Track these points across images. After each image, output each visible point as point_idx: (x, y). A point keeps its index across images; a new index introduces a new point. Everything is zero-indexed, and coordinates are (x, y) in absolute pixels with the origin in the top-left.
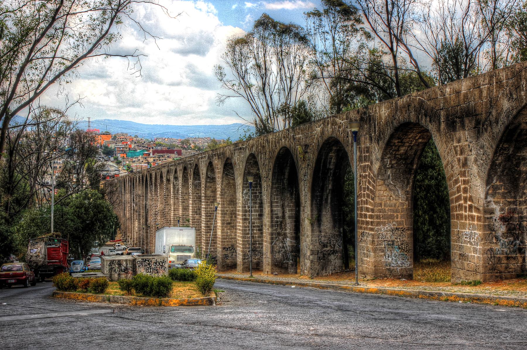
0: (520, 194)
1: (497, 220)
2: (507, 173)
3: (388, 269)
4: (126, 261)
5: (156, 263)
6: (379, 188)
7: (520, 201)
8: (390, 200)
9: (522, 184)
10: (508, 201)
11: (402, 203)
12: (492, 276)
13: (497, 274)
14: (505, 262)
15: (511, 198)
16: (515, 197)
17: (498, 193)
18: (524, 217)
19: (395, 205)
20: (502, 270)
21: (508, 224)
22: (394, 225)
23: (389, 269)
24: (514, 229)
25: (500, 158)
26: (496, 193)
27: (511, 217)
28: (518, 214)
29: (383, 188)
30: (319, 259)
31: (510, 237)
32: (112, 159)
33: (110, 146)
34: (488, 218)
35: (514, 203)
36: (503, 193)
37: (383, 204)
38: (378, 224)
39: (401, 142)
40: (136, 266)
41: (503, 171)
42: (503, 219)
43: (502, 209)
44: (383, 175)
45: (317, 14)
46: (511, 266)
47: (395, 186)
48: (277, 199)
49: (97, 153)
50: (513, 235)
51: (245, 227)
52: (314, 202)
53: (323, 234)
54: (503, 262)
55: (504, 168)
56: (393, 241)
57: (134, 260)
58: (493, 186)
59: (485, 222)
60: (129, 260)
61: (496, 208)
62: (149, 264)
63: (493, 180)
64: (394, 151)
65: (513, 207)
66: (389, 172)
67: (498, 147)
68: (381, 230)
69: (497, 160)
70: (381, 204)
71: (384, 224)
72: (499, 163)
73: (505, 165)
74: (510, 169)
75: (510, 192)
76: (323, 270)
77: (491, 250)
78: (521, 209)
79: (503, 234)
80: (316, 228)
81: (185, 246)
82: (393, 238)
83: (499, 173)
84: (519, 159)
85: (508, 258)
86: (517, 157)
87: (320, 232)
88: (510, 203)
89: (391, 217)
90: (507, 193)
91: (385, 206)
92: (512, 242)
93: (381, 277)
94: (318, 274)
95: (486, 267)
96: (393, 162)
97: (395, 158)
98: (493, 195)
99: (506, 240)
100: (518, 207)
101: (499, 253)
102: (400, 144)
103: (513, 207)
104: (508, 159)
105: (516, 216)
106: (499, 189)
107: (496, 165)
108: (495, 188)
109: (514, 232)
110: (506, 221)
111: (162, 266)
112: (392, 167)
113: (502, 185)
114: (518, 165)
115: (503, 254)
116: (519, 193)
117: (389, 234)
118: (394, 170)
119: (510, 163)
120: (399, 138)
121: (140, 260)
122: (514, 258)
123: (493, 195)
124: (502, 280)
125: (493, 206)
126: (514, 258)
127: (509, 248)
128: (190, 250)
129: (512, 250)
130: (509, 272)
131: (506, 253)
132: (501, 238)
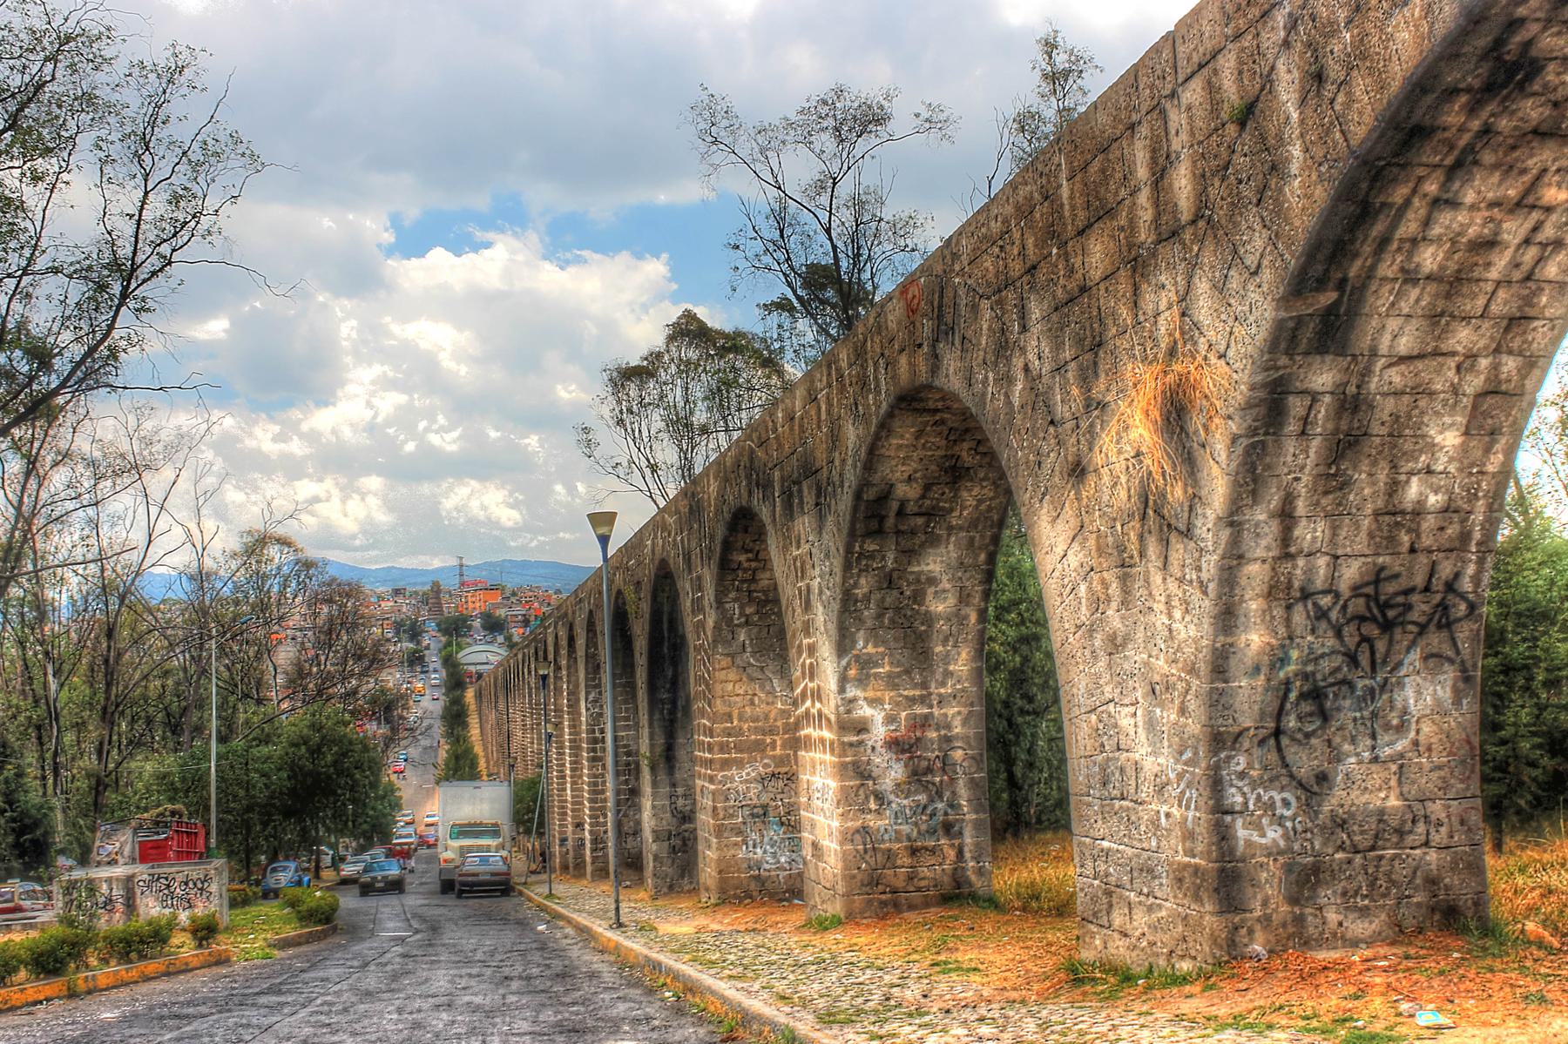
0: (939, 677)
1: (879, 749)
2: (892, 621)
3: (754, 877)
4: (109, 880)
5: (186, 884)
6: (721, 675)
7: (940, 695)
8: (752, 703)
9: (939, 649)
10: (907, 697)
11: (783, 711)
12: (870, 902)
13: (883, 897)
14: (907, 861)
15: (915, 686)
16: (924, 685)
17: (876, 675)
18: (957, 737)
19: (766, 717)
20: (900, 883)
21: (911, 758)
22: (766, 766)
23: (757, 878)
24: (929, 770)
25: (863, 581)
26: (868, 676)
27: (918, 740)
28: (937, 730)
29: (732, 675)
30: (673, 849)
31: (916, 792)
32: (500, 639)
33: (498, 613)
34: (851, 745)
35: (923, 700)
36: (890, 675)
37: (735, 715)
38: (726, 764)
39: (756, 559)
40: (134, 893)
41: (880, 616)
42: (894, 744)
43: (890, 719)
44: (727, 643)
45: (782, 306)
46: (924, 871)
47: (762, 668)
48: (627, 710)
49: (470, 628)
50: (925, 787)
51: (595, 776)
52: (657, 716)
53: (680, 790)
54: (899, 862)
55: (882, 610)
56: (765, 807)
57: (130, 878)
58: (857, 656)
59: (843, 754)
60: (117, 879)
61: (874, 716)
62: (168, 886)
63: (854, 642)
64: (743, 581)
65: (921, 710)
66: (742, 636)
67: (849, 550)
68: (732, 780)
69: (856, 585)
70: (729, 717)
71: (740, 764)
72: (864, 595)
73: (883, 599)
74: (898, 610)
75: (908, 672)
76: (682, 877)
77: (865, 830)
78: (946, 715)
79: (898, 785)
80: (662, 776)
81: (481, 824)
82: (765, 799)
83: (869, 623)
84: (918, 581)
85: (914, 852)
86: (911, 578)
87: (674, 785)
88: (912, 701)
89: (759, 747)
90: (899, 675)
91: (740, 720)
92: (925, 807)
93: (735, 896)
94: (671, 887)
95: (854, 877)
96: (748, 611)
97: (751, 600)
98: (860, 681)
99: (905, 802)
100: (936, 711)
101: (886, 837)
102: (754, 564)
103: (921, 710)
104: (889, 581)
105: (932, 734)
106: (877, 665)
107: (856, 601)
108: (865, 663)
109: (929, 778)
110: (903, 751)
111: (202, 889)
112: (747, 622)
113: (883, 655)
114: (918, 597)
115: (898, 840)
116: (933, 673)
117: (755, 788)
118: (755, 630)
119: (895, 593)
120: (747, 551)
121: (145, 877)
122: (933, 851)
123: (862, 682)
124: (900, 912)
125: (865, 711)
126: (933, 851)
127: (916, 824)
128: (494, 831)
129: (924, 827)
130: (919, 890)
131: (909, 839)
132: (892, 797)
